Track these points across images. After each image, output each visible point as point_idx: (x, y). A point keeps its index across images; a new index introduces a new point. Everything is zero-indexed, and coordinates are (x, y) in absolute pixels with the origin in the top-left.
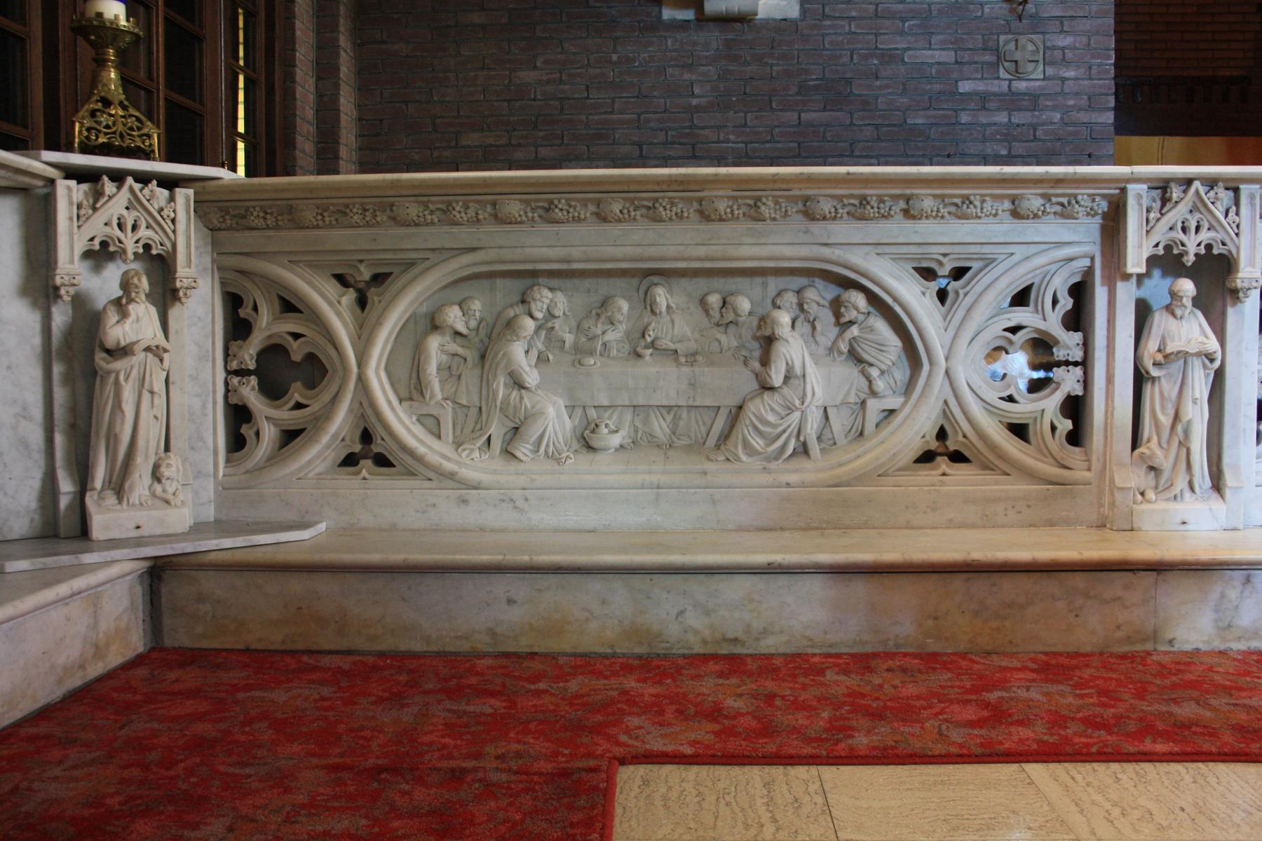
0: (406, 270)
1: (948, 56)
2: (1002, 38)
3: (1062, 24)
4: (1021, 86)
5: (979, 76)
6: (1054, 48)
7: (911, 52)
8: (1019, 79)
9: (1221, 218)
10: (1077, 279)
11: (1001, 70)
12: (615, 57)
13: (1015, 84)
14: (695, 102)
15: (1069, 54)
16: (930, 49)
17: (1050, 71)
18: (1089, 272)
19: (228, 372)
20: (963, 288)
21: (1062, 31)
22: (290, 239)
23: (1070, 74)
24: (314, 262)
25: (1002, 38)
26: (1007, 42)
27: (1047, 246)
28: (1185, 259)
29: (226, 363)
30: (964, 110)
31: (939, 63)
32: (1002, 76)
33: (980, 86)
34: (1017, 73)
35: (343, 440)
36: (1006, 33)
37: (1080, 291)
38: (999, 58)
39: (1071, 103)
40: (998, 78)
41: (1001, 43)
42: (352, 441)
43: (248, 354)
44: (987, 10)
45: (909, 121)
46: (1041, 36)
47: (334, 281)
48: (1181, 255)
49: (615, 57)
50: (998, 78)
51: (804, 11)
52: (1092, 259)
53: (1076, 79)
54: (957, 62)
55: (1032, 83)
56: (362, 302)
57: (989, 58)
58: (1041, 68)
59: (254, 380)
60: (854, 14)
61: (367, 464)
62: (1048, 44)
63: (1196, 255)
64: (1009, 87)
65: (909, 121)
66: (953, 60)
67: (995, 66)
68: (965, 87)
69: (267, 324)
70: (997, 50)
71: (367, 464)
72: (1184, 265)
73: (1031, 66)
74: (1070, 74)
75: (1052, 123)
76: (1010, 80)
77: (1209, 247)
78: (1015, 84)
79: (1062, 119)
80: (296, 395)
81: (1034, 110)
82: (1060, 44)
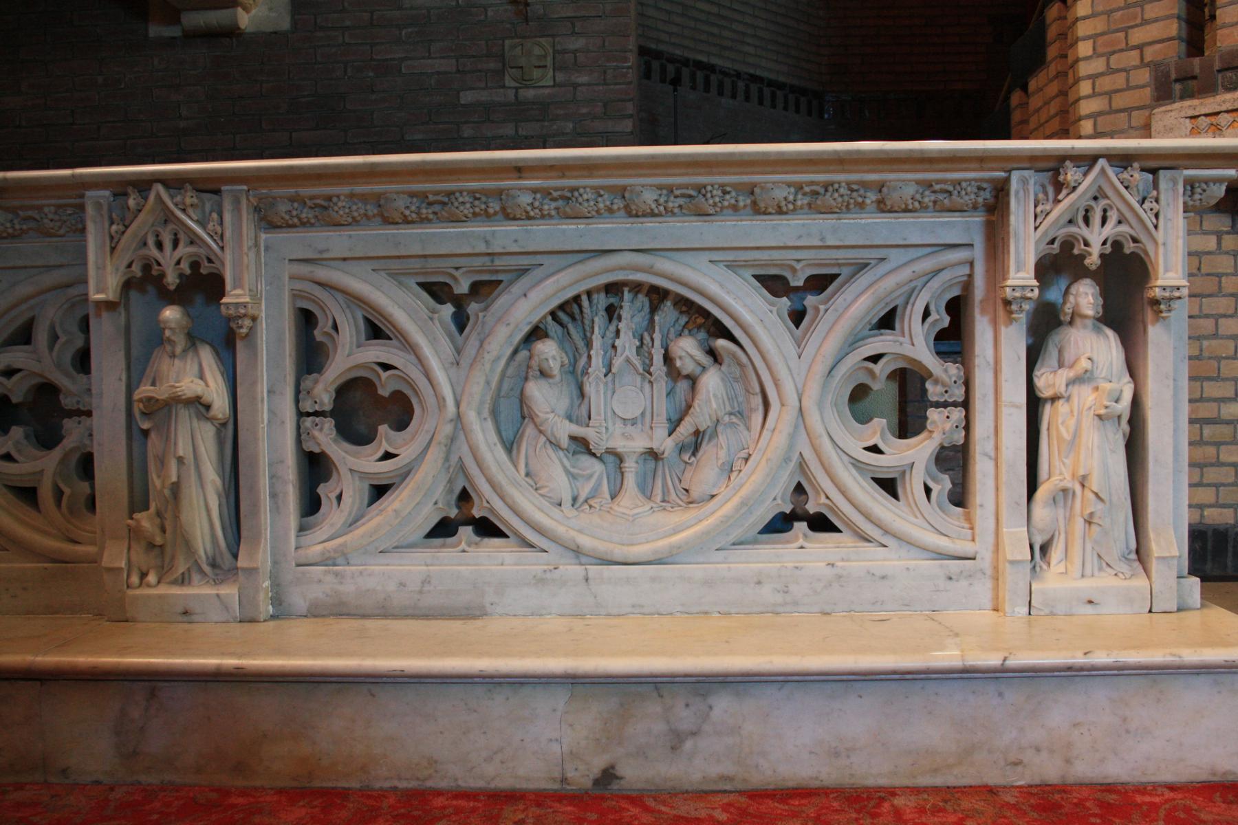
0: (519, 277)
1: (448, 65)
2: (507, 42)
3: (573, 25)
4: (530, 94)
5: (483, 85)
6: (564, 52)
7: (409, 62)
8: (527, 87)
9: (1136, 206)
10: (956, 292)
11: (507, 77)
12: (100, 79)
13: (521, 92)
14: (182, 124)
15: (581, 58)
16: (429, 58)
17: (560, 77)
18: (968, 285)
19: (301, 414)
20: (825, 303)
21: (573, 33)
22: (375, 239)
23: (583, 79)
24: (392, 266)
25: (507, 42)
26: (513, 47)
27: (929, 250)
28: (1087, 262)
29: (297, 401)
30: (466, 122)
31: (438, 73)
32: (507, 84)
33: (484, 96)
34: (525, 82)
35: (436, 503)
36: (512, 38)
37: (957, 308)
38: (504, 65)
39: (584, 111)
40: (504, 87)
41: (506, 47)
42: (448, 504)
43: (323, 391)
44: (490, 13)
45: (407, 137)
46: (550, 39)
47: (425, 295)
48: (1082, 257)
49: (100, 79)
50: (504, 87)
51: (294, 23)
52: (972, 264)
53: (589, 85)
54: (458, 71)
55: (541, 91)
56: (461, 321)
57: (492, 65)
58: (551, 73)
59: (329, 423)
60: (348, 23)
61: (466, 532)
62: (558, 47)
63: (1102, 256)
64: (516, 96)
65: (407, 137)
66: (454, 70)
67: (500, 73)
68: (467, 97)
69: (350, 354)
70: (503, 56)
71: (466, 532)
72: (1087, 268)
73: (536, 73)
74: (583, 79)
75: (563, 134)
76: (517, 89)
77: (1117, 245)
78: (521, 92)
79: (575, 128)
80: (384, 442)
81: (543, 121)
82: (572, 47)
